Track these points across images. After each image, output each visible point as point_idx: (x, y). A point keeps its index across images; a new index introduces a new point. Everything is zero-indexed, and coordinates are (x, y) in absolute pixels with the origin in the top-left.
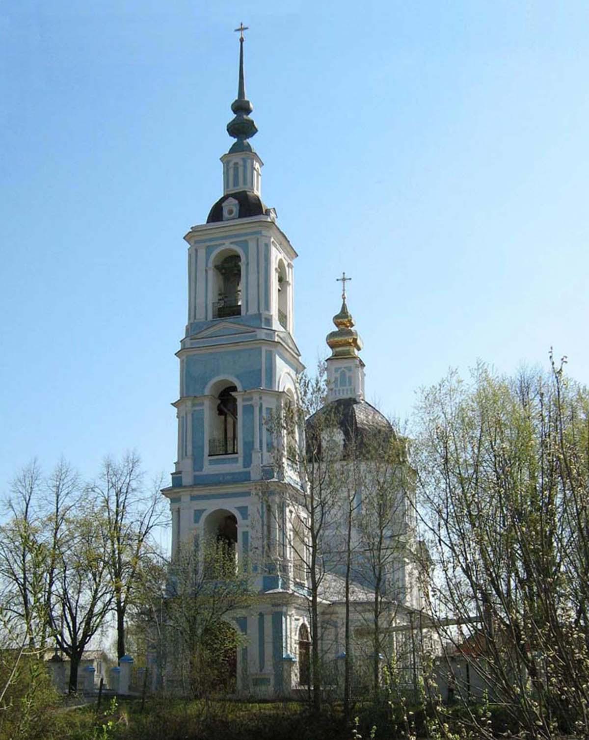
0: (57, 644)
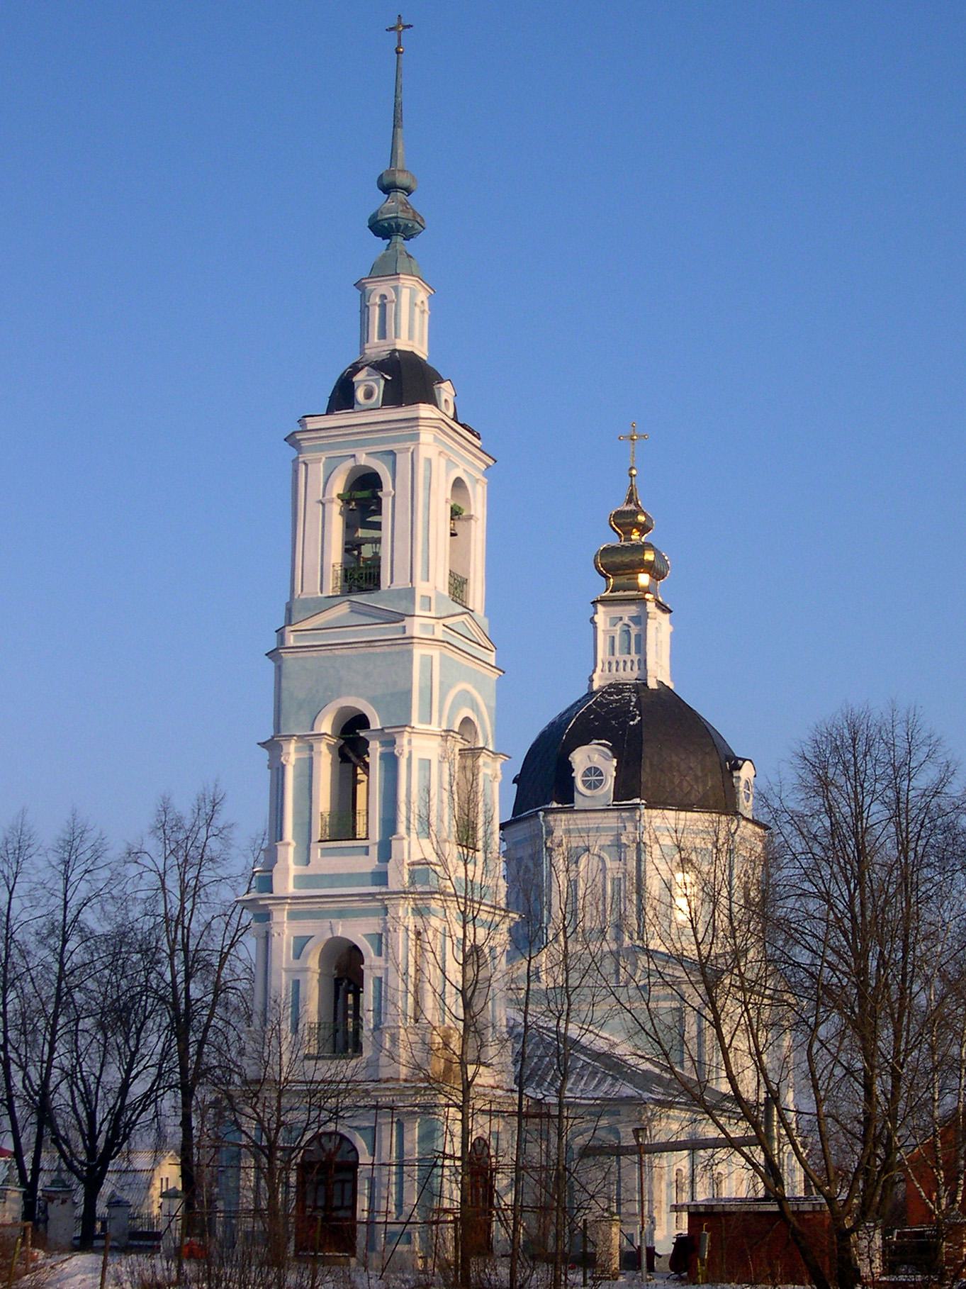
0: (59, 1158)
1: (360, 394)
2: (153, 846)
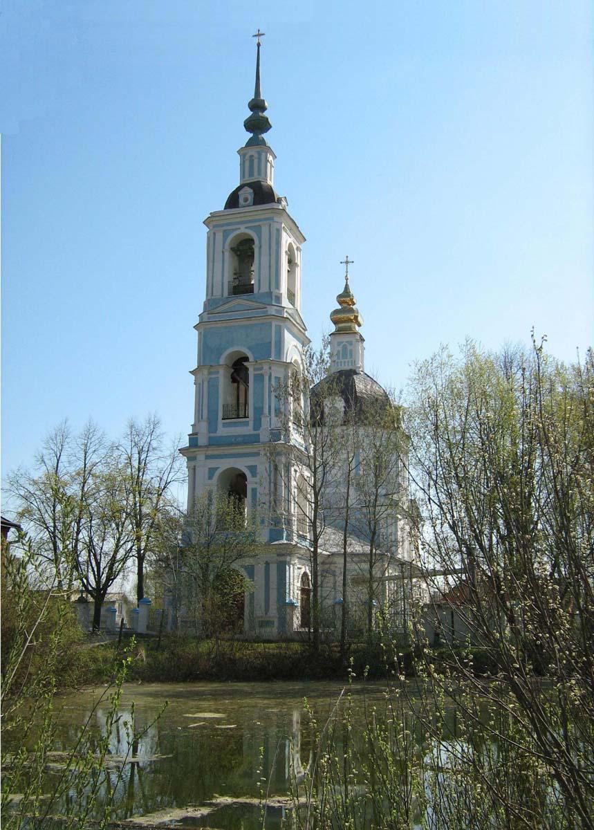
1: (241, 201)
2: (126, 444)
